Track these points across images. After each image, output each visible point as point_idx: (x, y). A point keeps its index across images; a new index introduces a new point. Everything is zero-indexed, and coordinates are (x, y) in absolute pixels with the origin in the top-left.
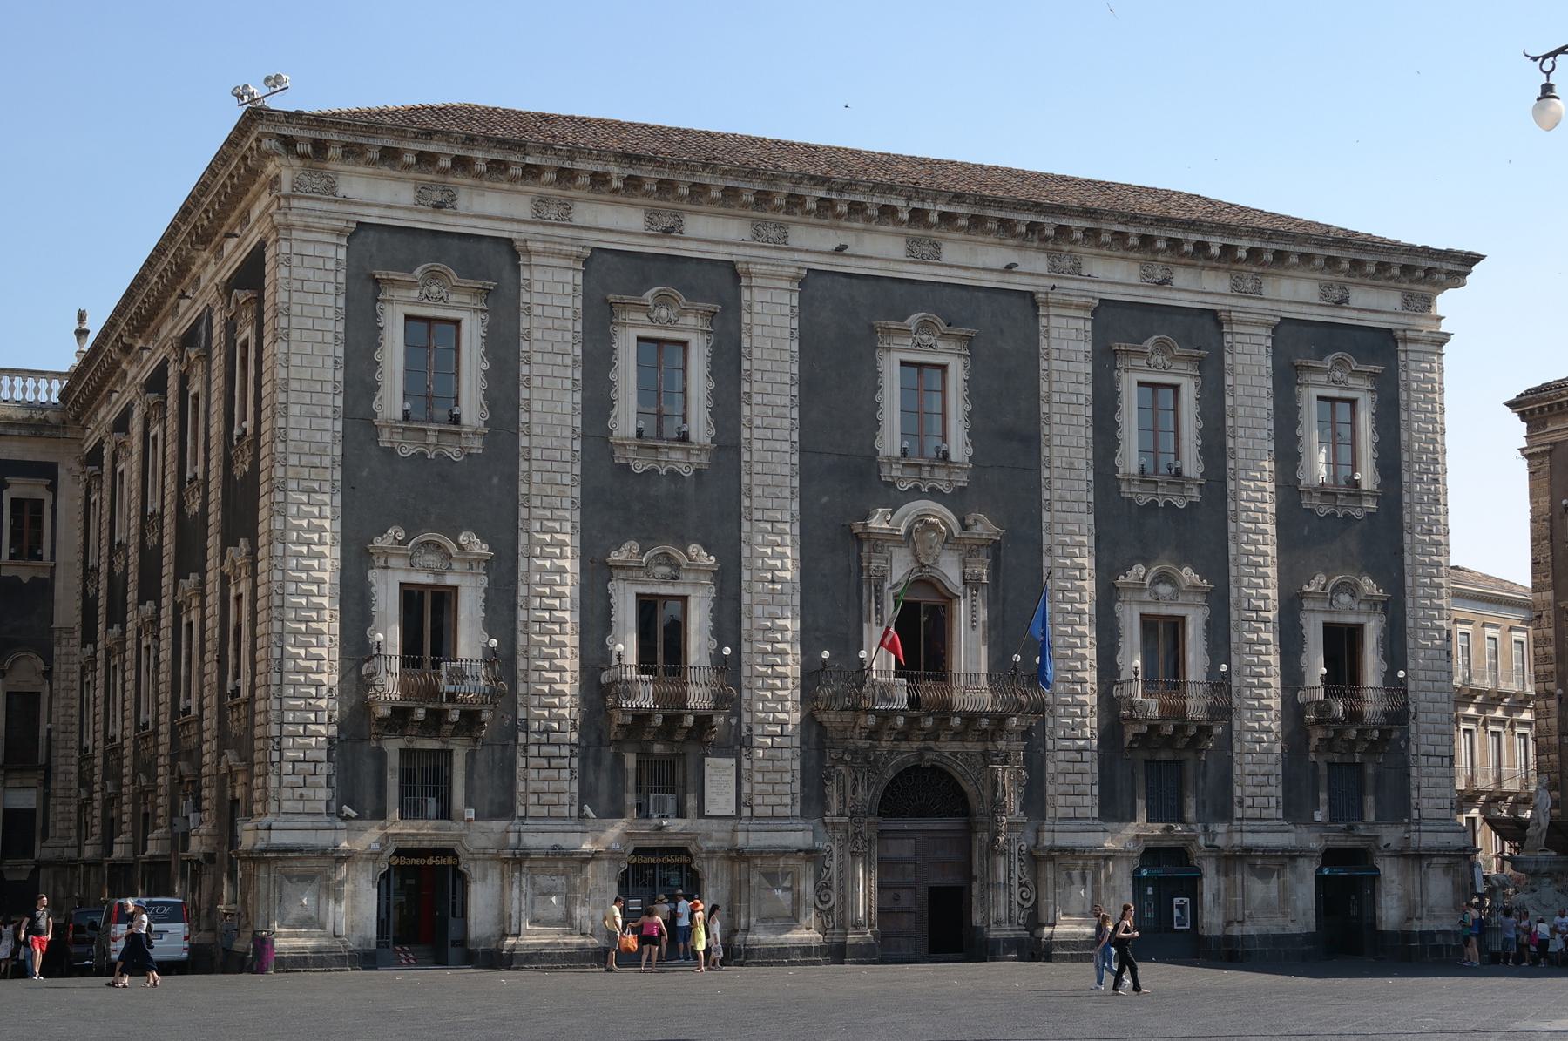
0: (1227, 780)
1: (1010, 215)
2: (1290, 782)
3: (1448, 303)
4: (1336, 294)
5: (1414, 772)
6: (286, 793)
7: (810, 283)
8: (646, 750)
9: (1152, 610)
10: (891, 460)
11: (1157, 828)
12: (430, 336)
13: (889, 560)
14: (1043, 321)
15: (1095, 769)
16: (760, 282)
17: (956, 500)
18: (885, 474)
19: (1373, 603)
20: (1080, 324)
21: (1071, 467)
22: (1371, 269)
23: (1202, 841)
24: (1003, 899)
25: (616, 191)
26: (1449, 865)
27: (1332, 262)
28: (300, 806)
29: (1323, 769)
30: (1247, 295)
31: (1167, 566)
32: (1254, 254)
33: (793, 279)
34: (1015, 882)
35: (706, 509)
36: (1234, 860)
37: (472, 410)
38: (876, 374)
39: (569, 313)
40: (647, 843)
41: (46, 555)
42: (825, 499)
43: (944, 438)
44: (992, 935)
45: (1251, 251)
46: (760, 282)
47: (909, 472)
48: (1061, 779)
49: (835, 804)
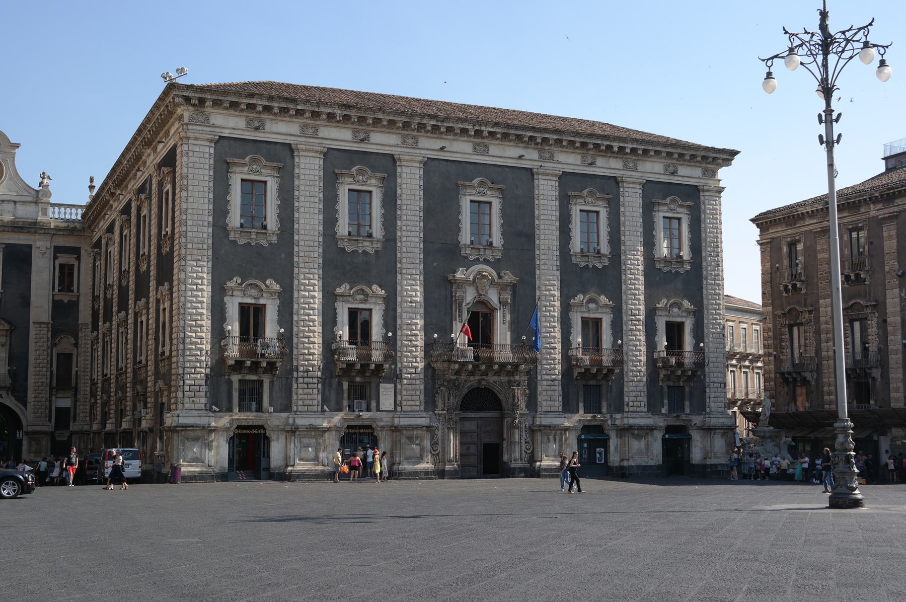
0: (621, 394)
2: (650, 395)
3: (723, 173)
4: (672, 169)
5: (707, 390)
6: (186, 400)
7: (428, 163)
8: (354, 379)
9: (586, 315)
10: (466, 246)
11: (589, 416)
13: (465, 292)
14: (536, 182)
16: (405, 164)
17: (496, 265)
18: (463, 252)
19: (688, 312)
21: (549, 249)
22: (688, 157)
23: (609, 422)
24: (517, 449)
25: (339, 121)
26: (723, 434)
27: (669, 154)
28: (192, 406)
29: (666, 389)
30: (631, 170)
31: (593, 295)
32: (634, 151)
33: (420, 162)
34: (523, 441)
35: (381, 268)
36: (625, 431)
37: (272, 223)
38: (459, 206)
39: (317, 178)
40: (353, 423)
41: (75, 290)
42: (435, 264)
43: (490, 236)
44: (512, 466)
46: (405, 164)
47: (474, 251)
48: (544, 393)
49: (440, 405)
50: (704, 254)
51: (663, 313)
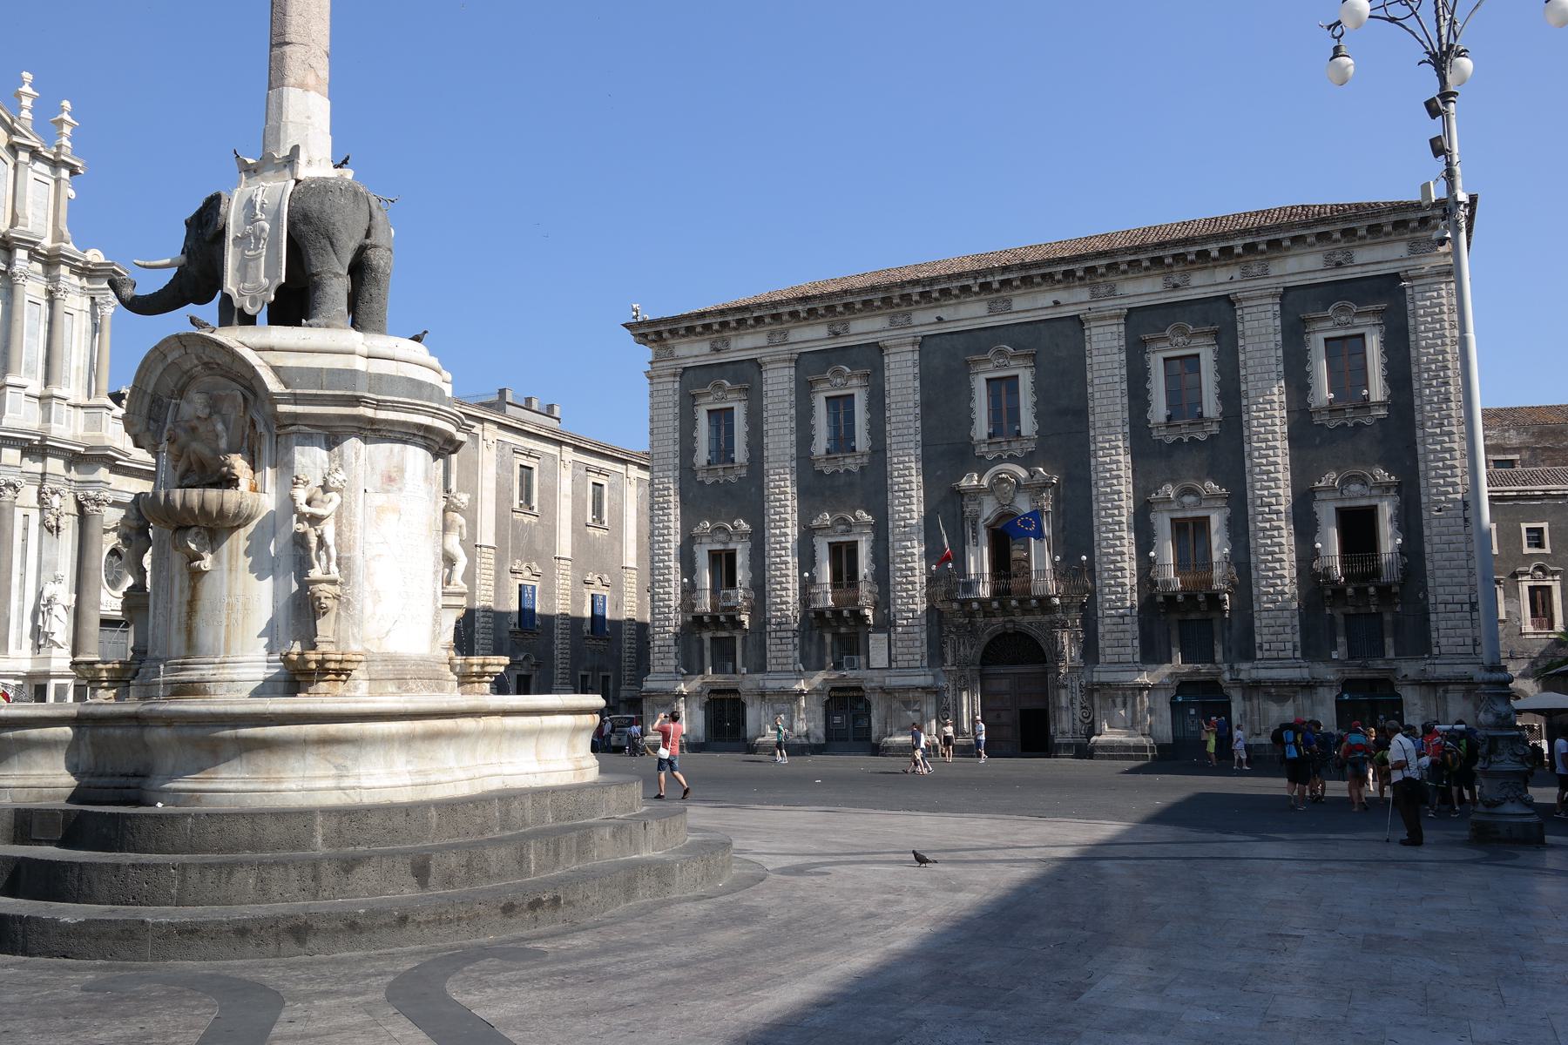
0: (1249, 632)
1: (1048, 270)
5: (1433, 617)
7: (924, 343)
8: (835, 632)
9: (1179, 515)
10: (1158, 426)
11: (1187, 668)
12: (841, 406)
15: (1136, 628)
17: (1027, 461)
19: (1385, 488)
20: (1114, 328)
21: (1109, 426)
23: (1227, 676)
25: (1147, 269)
29: (1340, 620)
32: (1250, 248)
33: (913, 344)
35: (872, 488)
38: (971, 391)
45: (1245, 247)
47: (993, 447)
48: (1108, 636)
49: (950, 659)
50: (1416, 385)
51: (1330, 495)
